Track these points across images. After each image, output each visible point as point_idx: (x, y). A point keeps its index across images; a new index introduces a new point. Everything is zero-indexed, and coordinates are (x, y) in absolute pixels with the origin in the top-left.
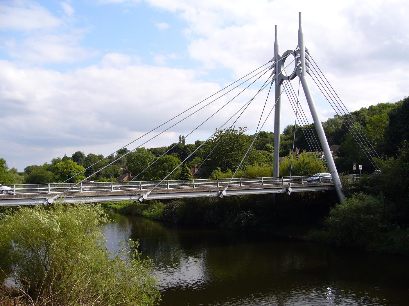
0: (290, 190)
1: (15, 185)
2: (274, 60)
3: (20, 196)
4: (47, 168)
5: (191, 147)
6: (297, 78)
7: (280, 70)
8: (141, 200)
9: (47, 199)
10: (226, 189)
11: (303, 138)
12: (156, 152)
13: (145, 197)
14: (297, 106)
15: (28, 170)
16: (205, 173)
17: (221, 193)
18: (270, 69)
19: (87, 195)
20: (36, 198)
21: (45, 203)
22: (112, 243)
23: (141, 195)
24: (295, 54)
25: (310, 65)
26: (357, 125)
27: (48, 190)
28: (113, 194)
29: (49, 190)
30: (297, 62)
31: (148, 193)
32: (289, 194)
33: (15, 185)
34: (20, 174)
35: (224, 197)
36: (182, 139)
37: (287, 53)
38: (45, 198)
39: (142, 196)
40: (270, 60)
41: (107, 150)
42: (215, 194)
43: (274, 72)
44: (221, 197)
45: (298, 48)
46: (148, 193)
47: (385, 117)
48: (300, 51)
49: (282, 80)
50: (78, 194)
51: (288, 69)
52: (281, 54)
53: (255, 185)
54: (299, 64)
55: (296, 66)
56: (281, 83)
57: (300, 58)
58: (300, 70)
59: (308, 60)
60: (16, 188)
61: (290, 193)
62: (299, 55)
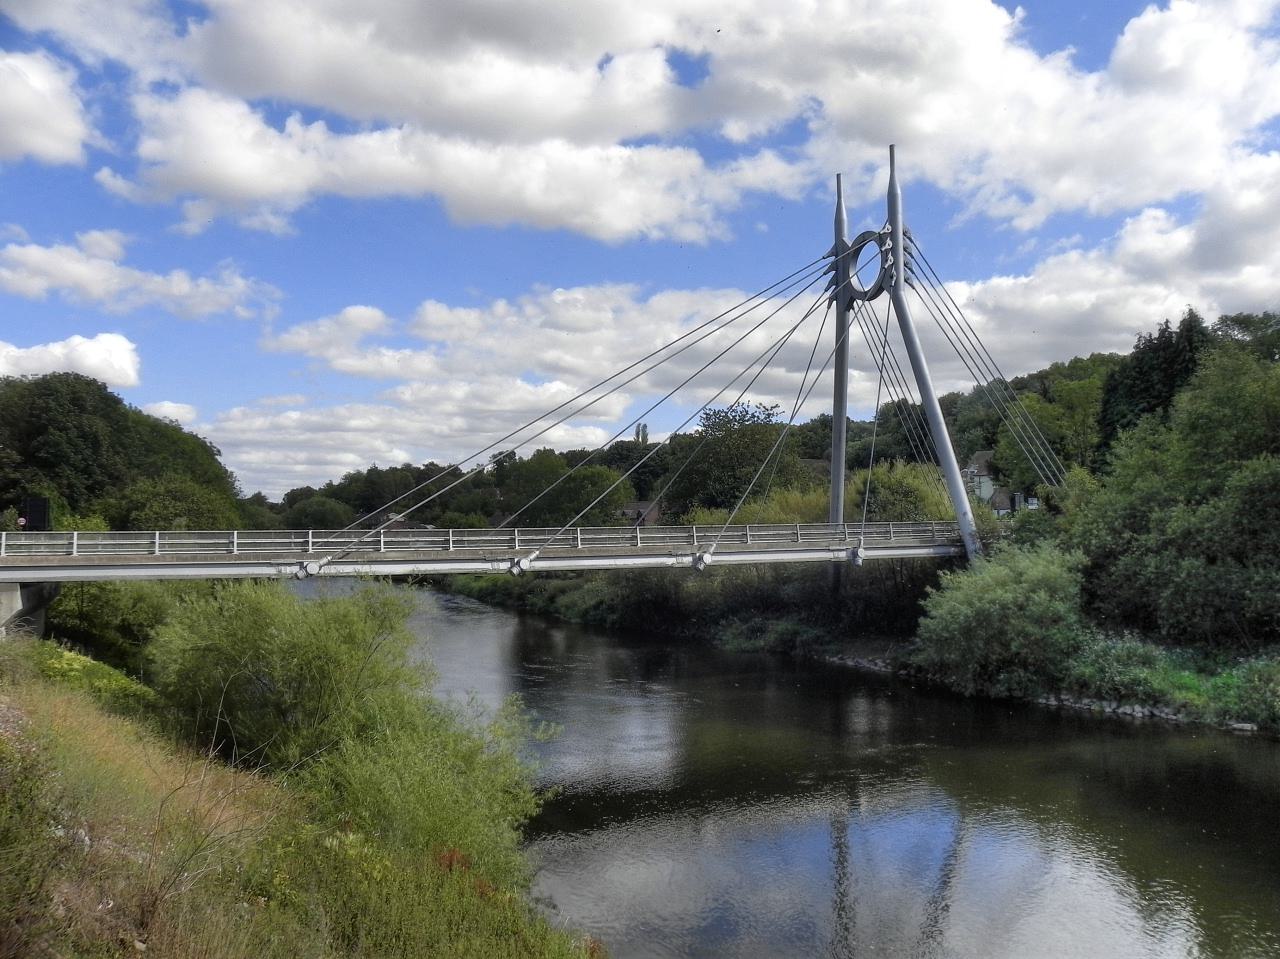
0: (863, 554)
1: (310, 532)
2: (835, 252)
3: (247, 557)
4: (331, 491)
5: (662, 451)
6: (885, 297)
7: (847, 276)
8: (515, 571)
9: (305, 564)
10: (712, 550)
11: (905, 433)
12: (575, 457)
13: (525, 564)
14: (885, 352)
15: (293, 497)
16: (676, 513)
17: (701, 558)
18: (825, 274)
19: (395, 555)
20: (281, 561)
21: (301, 574)
22: (465, 674)
23: (516, 560)
24: (881, 239)
25: (914, 252)
26: (1029, 400)
27: (313, 542)
28: (453, 556)
29: (310, 544)
30: (885, 260)
31: (533, 556)
32: (860, 562)
33: (157, 533)
34: (273, 507)
35: (708, 567)
36: (642, 430)
37: (864, 238)
38: (302, 563)
39: (518, 562)
40: (825, 254)
41: (472, 457)
42: (688, 560)
43: (835, 282)
44: (701, 567)
45: (888, 226)
46: (533, 556)
47: (1097, 381)
48: (893, 235)
49: (852, 300)
50: (374, 556)
51: (863, 277)
52: (849, 240)
53: (197, 552)
54: (889, 263)
55: (883, 267)
56: (850, 306)
57: (894, 250)
58: (892, 277)
59: (910, 254)
60: (313, 537)
61: (860, 561)
62: (889, 241)
